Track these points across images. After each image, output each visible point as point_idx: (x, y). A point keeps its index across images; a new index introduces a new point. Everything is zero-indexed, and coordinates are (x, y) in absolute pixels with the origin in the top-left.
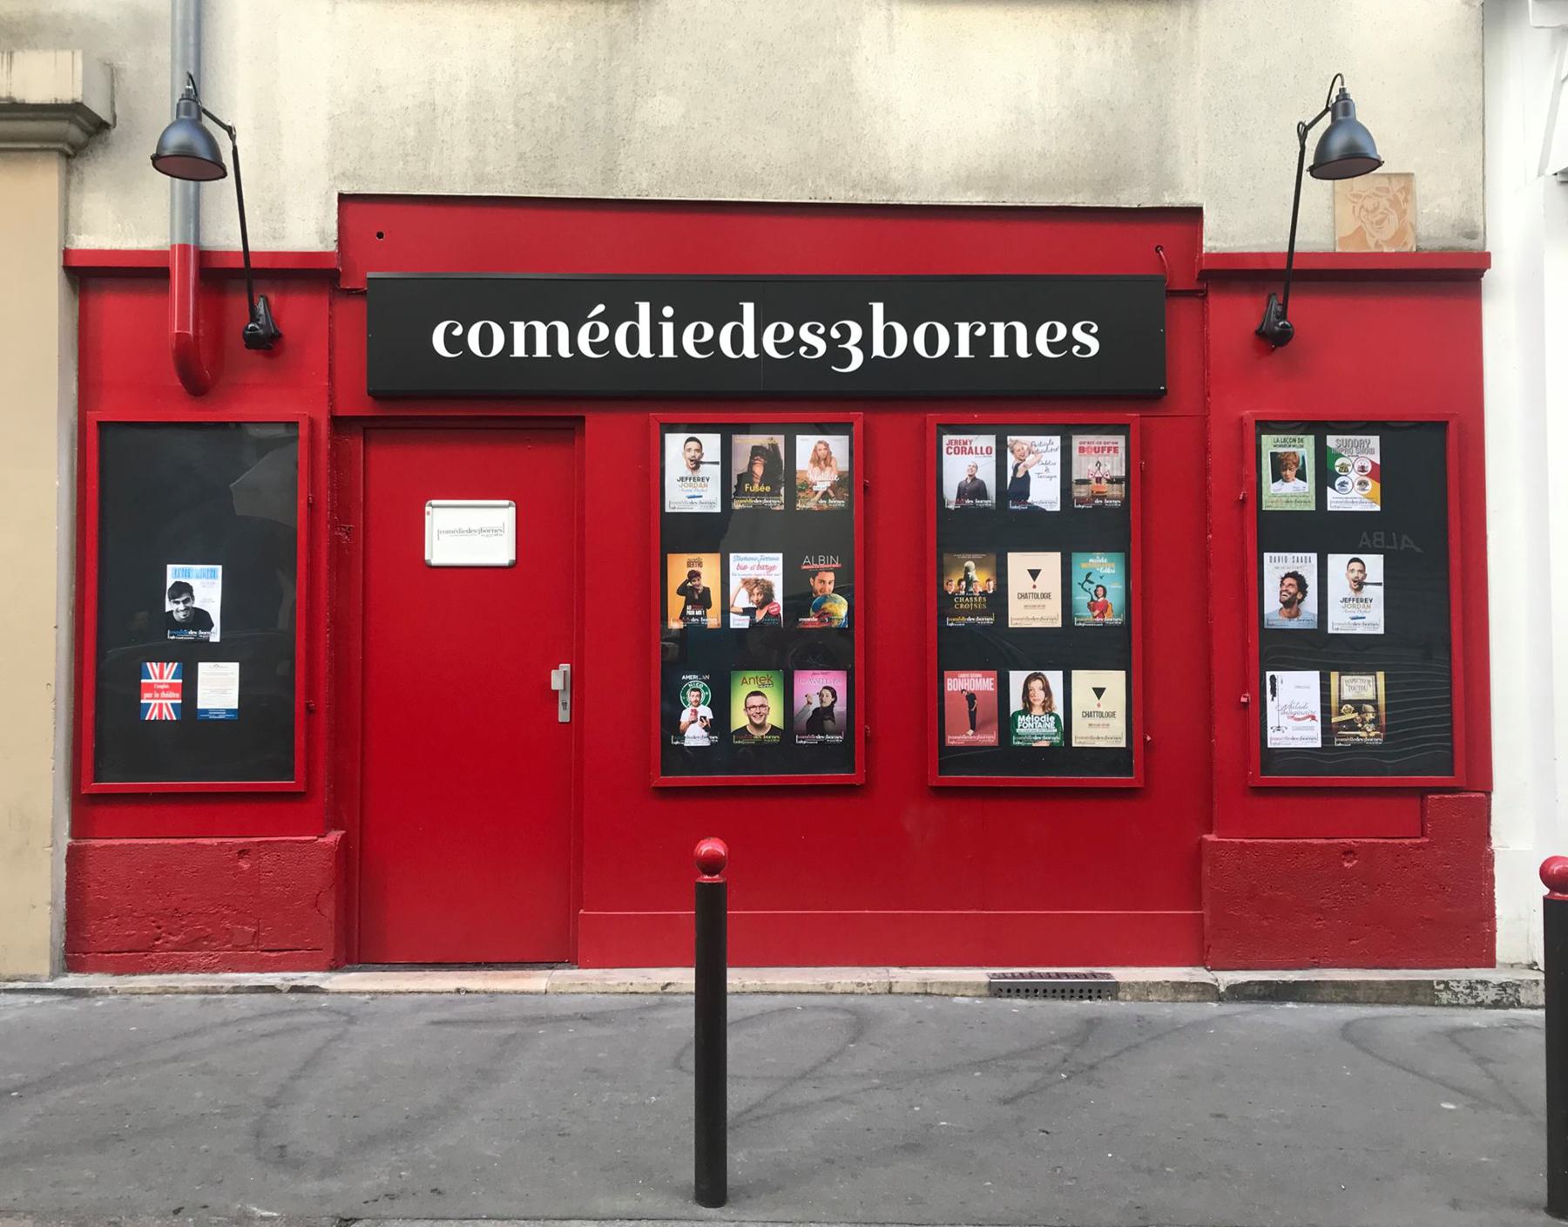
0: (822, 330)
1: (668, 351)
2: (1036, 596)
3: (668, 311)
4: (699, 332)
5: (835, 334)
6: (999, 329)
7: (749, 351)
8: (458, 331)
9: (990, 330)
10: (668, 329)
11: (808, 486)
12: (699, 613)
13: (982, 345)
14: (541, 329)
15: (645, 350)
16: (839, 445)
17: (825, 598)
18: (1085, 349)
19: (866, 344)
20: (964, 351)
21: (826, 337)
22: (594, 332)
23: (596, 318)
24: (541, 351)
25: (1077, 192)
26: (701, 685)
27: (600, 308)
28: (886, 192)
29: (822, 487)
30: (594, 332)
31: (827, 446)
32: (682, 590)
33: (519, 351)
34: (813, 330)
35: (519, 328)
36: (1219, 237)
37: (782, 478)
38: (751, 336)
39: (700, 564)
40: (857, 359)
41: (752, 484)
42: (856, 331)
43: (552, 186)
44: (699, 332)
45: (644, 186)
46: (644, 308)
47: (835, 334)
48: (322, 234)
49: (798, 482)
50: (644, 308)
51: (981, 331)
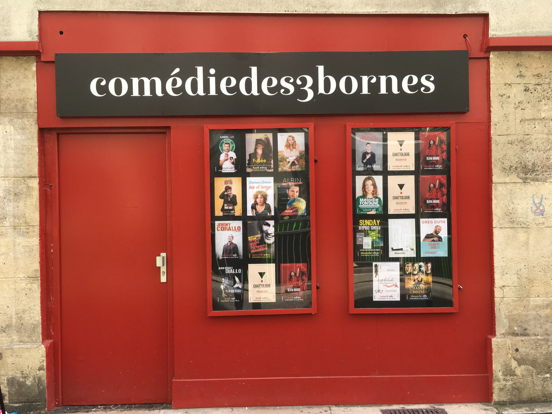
0: (292, 81)
1: (213, 92)
2: (402, 198)
3: (212, 71)
4: (229, 82)
5: (299, 82)
6: (383, 79)
7: (255, 92)
8: (103, 83)
9: (378, 80)
10: (212, 80)
11: (284, 159)
12: (231, 208)
13: (374, 87)
14: (147, 82)
15: (201, 92)
16: (299, 138)
17: (294, 201)
18: (427, 89)
19: (315, 87)
20: (365, 91)
21: (294, 84)
22: (174, 83)
23: (176, 75)
24: (147, 93)
25: (424, 6)
26: (230, 141)
27: (177, 70)
28: (325, 7)
29: (291, 159)
30: (174, 83)
31: (293, 138)
32: (222, 196)
33: (136, 93)
34: (287, 80)
35: (135, 81)
36: (498, 29)
37: (272, 155)
38: (255, 84)
39: (231, 183)
40: (311, 95)
41: (256, 159)
42: (310, 81)
43: (151, 5)
44: (229, 82)
45: (199, 5)
46: (200, 70)
47: (299, 82)
48: (30, 32)
49: (279, 157)
50: (200, 70)
51: (374, 80)
